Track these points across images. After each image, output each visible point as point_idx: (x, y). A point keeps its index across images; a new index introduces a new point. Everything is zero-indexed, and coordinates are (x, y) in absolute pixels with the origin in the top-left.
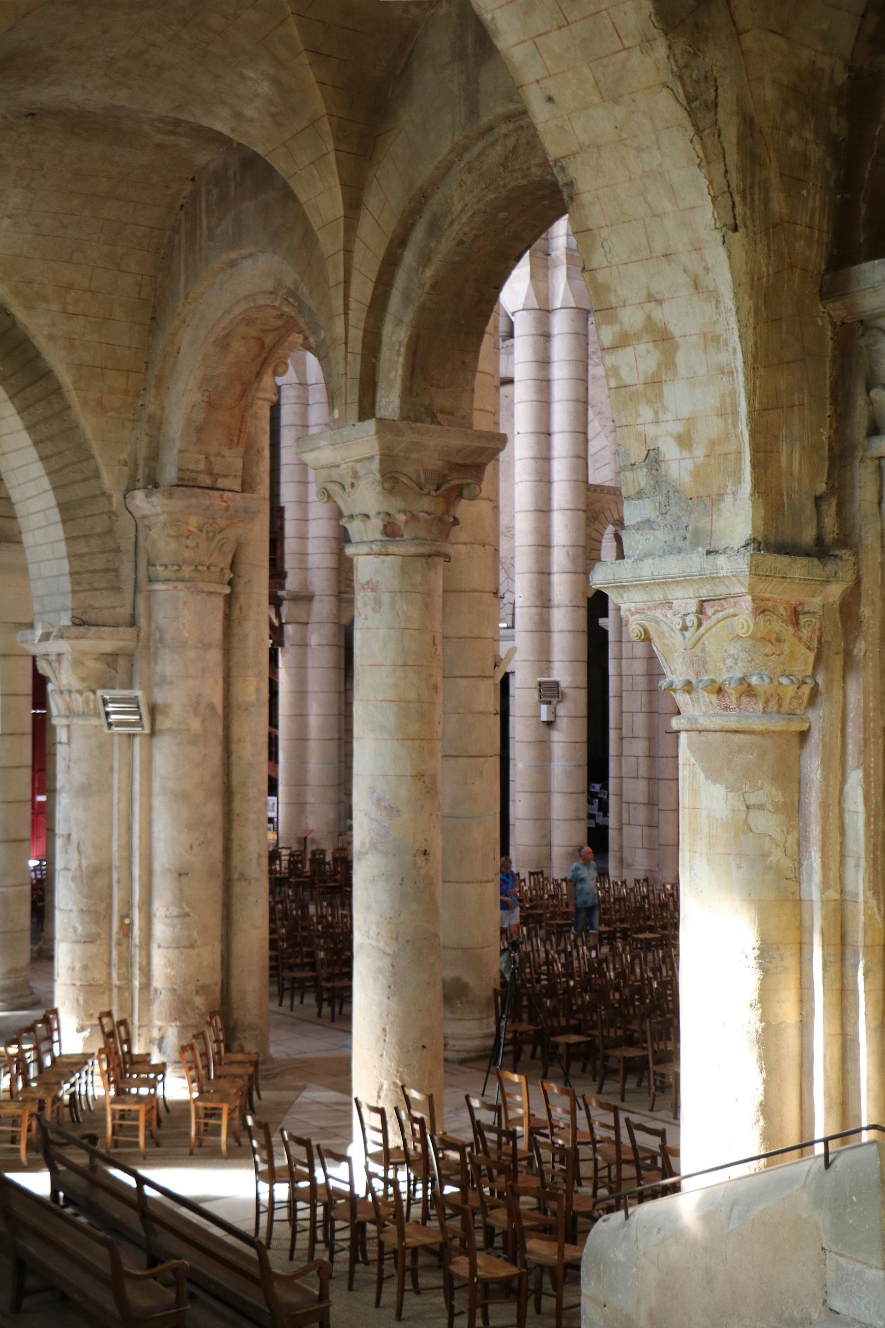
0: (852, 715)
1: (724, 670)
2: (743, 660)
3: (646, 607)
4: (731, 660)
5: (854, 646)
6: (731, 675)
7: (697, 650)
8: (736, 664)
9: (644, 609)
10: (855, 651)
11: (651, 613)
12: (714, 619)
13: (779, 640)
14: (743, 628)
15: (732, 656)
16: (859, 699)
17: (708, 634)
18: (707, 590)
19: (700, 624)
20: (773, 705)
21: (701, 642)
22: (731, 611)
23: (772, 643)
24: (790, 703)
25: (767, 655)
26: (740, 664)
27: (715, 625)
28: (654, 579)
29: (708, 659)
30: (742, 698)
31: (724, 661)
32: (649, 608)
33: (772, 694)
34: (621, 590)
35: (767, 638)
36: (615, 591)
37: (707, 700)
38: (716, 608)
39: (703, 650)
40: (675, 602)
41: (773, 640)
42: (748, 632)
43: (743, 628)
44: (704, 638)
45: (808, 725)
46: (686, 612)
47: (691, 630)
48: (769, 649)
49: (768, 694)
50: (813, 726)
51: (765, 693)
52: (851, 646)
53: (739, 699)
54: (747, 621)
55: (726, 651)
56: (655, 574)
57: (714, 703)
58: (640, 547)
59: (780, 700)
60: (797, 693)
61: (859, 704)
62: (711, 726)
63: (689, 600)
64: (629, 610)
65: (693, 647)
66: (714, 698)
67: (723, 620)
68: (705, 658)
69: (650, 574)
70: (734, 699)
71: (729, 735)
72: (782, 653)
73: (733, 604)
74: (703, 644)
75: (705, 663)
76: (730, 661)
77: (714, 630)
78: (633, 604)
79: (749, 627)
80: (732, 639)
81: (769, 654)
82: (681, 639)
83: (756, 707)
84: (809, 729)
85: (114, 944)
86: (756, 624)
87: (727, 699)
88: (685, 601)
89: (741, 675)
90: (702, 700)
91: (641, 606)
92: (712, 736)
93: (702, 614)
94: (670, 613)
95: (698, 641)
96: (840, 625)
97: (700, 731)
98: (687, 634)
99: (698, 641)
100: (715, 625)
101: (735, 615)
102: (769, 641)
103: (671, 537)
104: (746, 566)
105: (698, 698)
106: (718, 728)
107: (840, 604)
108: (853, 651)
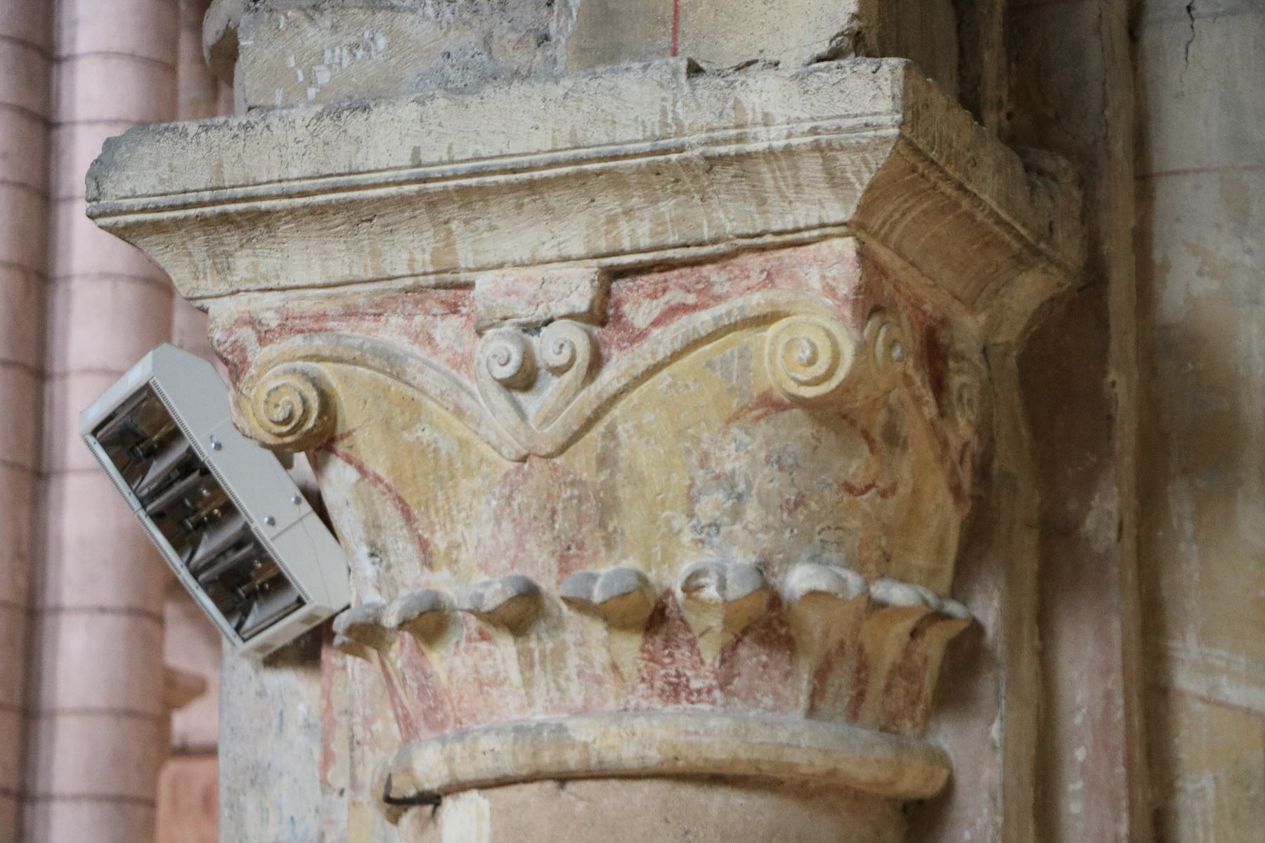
0: (1080, 754)
1: (687, 538)
2: (764, 503)
3: (332, 308)
4: (720, 496)
5: (1086, 505)
6: (708, 557)
7: (580, 461)
8: (736, 514)
9: (323, 316)
10: (1090, 523)
11: (358, 333)
12: (666, 338)
13: (893, 437)
14: (811, 361)
15: (725, 481)
16: (1108, 696)
17: (635, 396)
18: (658, 220)
19: (596, 363)
20: (841, 680)
21: (600, 428)
22: (757, 301)
23: (871, 442)
24: (888, 689)
25: (849, 489)
26: (752, 513)
27: (675, 356)
28: (425, 180)
29: (625, 493)
30: (743, 651)
31: (692, 500)
32: (350, 313)
33: (842, 645)
34: (232, 238)
35: (400, 651)
36: (198, 246)
37: (600, 657)
38: (675, 296)
39: (605, 460)
40: (484, 282)
41: (876, 432)
42: (817, 382)
43: (811, 361)
44: (616, 412)
45: (943, 774)
46: (540, 314)
47: (551, 388)
48: (857, 467)
49: (833, 642)
50: (962, 780)
51: (826, 634)
52: (1073, 505)
53: (728, 654)
54: (829, 334)
55: (704, 461)
56: (426, 157)
57: (628, 669)
58: (324, 77)
59: (863, 668)
60: (907, 652)
61: (1107, 711)
62: (629, 754)
63: (556, 270)
64: (252, 322)
65: (562, 449)
66: (630, 647)
67: (710, 338)
68: (609, 488)
69: (404, 158)
70: (710, 652)
71: (688, 792)
72: (893, 489)
73: (756, 278)
74: (611, 433)
75: (608, 507)
76: (711, 505)
77: (664, 377)
78: (274, 299)
79: (836, 357)
80: (736, 417)
81: (858, 482)
82: (513, 419)
83: (786, 692)
84: (948, 792)
85: (837, 121)
86: (863, 349)
87: (683, 653)
88: (537, 272)
89: (753, 559)
90: (573, 660)
91: (309, 303)
92: (612, 795)
93: (603, 323)
94: (447, 330)
95: (589, 423)
96: (1024, 431)
97: (563, 779)
98: (531, 403)
99: (589, 423)
100: (675, 356)
101: (763, 320)
102: (866, 434)
103: (472, 38)
104: (885, 105)
105: (559, 655)
106: (654, 757)
107: (1021, 360)
108: (1079, 522)
